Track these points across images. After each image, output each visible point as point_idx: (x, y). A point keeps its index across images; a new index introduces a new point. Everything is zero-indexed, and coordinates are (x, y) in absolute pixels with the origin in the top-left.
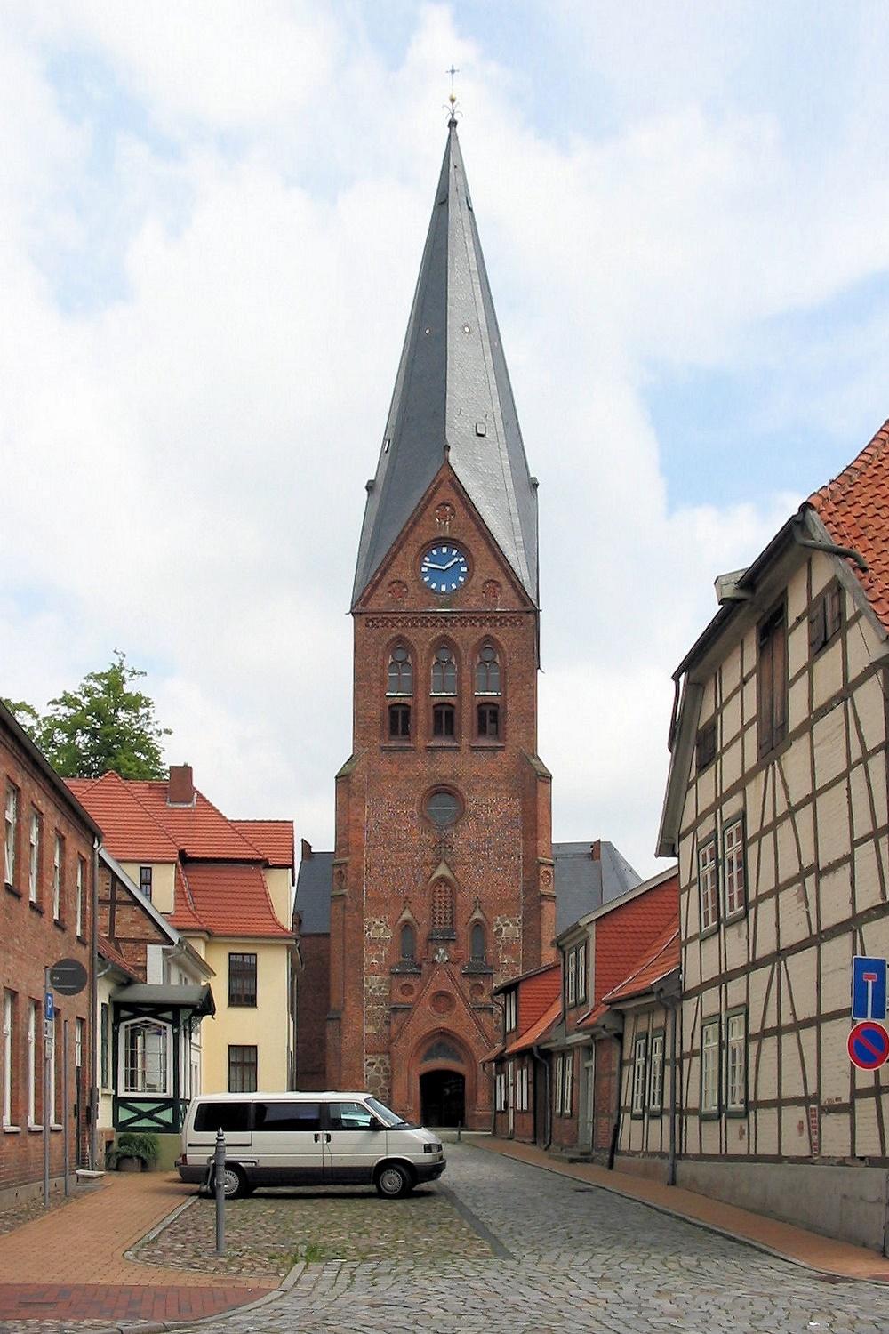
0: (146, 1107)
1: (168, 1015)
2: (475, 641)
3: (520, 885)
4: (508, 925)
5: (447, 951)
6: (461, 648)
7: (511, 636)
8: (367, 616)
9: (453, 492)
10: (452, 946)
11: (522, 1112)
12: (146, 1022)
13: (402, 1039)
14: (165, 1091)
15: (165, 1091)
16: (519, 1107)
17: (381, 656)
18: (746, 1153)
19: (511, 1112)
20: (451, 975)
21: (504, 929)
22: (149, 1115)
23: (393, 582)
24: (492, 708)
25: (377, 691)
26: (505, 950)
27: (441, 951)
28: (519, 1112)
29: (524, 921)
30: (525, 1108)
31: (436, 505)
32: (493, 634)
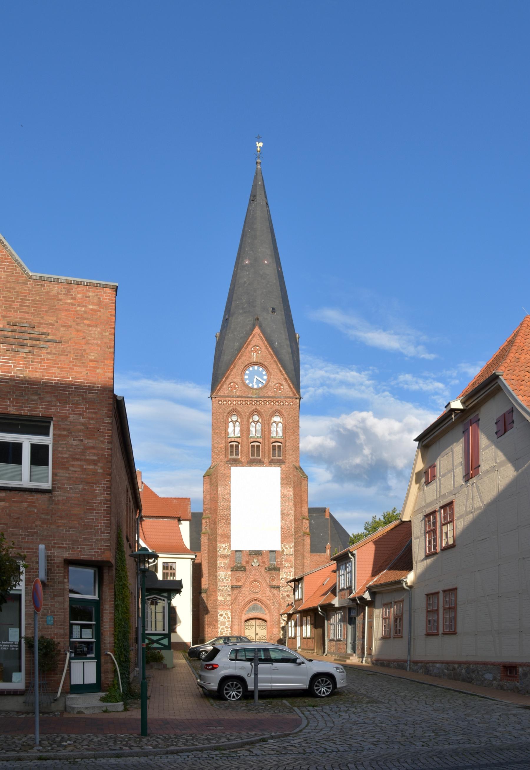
0: (155, 638)
1: (166, 594)
2: (270, 412)
3: (293, 529)
4: (287, 548)
5: (258, 561)
6: (264, 415)
7: (288, 410)
8: (219, 398)
9: (260, 340)
10: (260, 557)
11: (307, 638)
12: (155, 597)
13: (237, 603)
14: (164, 630)
15: (164, 630)
16: (304, 635)
17: (225, 419)
18: (82, 683)
19: (298, 639)
20: (260, 572)
21: (285, 550)
22: (157, 641)
23: (231, 383)
24: (237, 444)
25: (223, 435)
26: (286, 560)
27: (255, 561)
28: (304, 638)
29: (295, 546)
30: (309, 635)
31: (252, 346)
32: (279, 409)
